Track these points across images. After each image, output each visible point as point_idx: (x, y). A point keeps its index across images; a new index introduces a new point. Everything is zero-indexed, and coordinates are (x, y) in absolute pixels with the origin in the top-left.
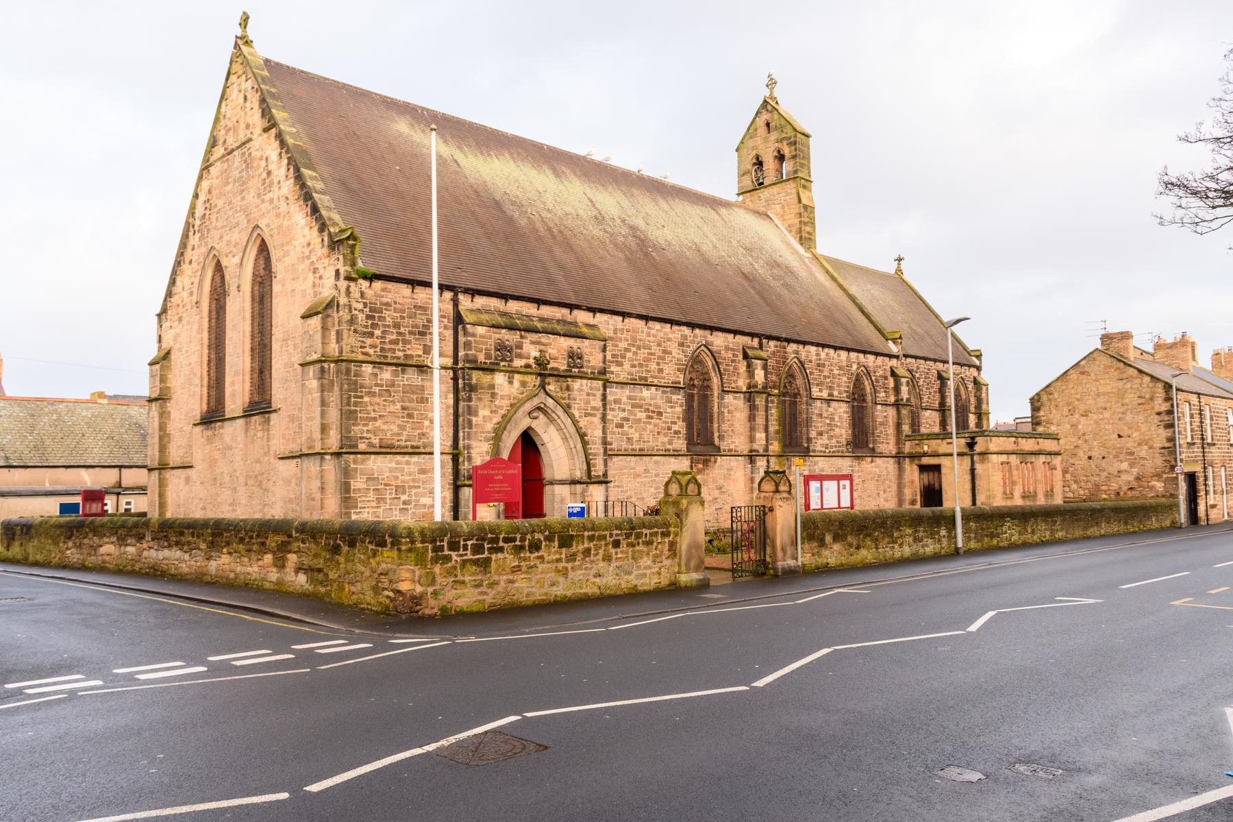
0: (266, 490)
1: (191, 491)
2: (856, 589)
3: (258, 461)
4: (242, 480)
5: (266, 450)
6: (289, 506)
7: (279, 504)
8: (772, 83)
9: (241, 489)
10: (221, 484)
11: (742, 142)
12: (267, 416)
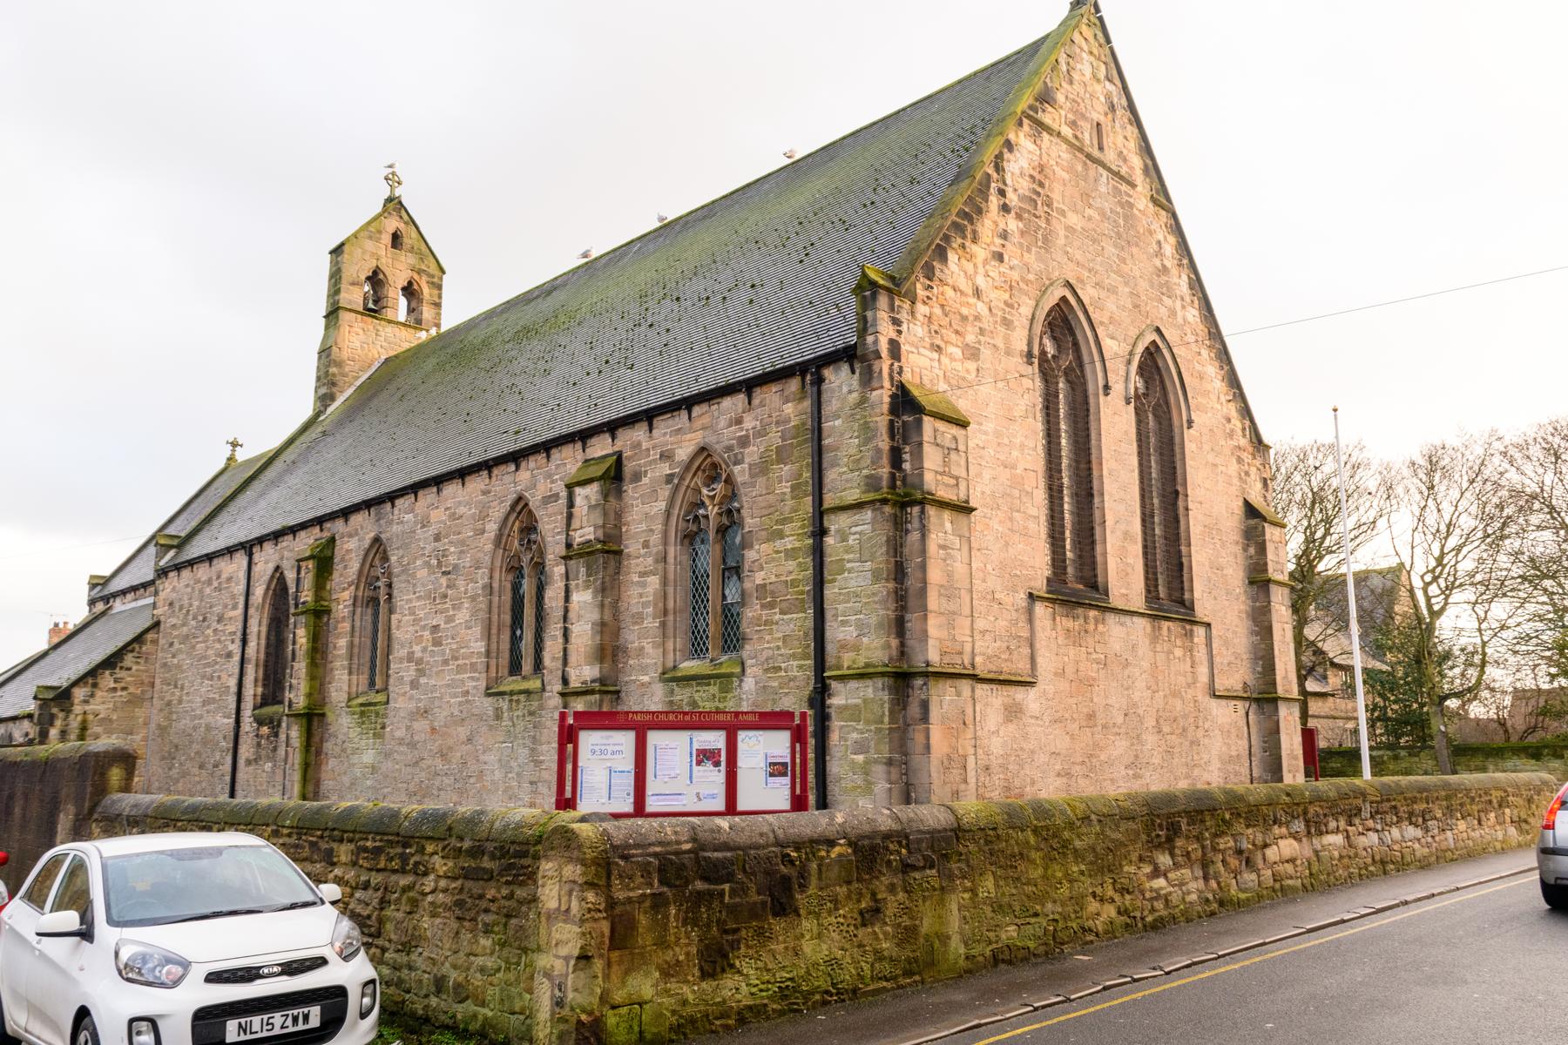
1: (1025, 737)
3: (1175, 694)
5: (1190, 680)
6: (1230, 768)
7: (1216, 764)
8: (392, 179)
9: (1150, 739)
10: (1104, 727)
11: (355, 235)
12: (1188, 627)
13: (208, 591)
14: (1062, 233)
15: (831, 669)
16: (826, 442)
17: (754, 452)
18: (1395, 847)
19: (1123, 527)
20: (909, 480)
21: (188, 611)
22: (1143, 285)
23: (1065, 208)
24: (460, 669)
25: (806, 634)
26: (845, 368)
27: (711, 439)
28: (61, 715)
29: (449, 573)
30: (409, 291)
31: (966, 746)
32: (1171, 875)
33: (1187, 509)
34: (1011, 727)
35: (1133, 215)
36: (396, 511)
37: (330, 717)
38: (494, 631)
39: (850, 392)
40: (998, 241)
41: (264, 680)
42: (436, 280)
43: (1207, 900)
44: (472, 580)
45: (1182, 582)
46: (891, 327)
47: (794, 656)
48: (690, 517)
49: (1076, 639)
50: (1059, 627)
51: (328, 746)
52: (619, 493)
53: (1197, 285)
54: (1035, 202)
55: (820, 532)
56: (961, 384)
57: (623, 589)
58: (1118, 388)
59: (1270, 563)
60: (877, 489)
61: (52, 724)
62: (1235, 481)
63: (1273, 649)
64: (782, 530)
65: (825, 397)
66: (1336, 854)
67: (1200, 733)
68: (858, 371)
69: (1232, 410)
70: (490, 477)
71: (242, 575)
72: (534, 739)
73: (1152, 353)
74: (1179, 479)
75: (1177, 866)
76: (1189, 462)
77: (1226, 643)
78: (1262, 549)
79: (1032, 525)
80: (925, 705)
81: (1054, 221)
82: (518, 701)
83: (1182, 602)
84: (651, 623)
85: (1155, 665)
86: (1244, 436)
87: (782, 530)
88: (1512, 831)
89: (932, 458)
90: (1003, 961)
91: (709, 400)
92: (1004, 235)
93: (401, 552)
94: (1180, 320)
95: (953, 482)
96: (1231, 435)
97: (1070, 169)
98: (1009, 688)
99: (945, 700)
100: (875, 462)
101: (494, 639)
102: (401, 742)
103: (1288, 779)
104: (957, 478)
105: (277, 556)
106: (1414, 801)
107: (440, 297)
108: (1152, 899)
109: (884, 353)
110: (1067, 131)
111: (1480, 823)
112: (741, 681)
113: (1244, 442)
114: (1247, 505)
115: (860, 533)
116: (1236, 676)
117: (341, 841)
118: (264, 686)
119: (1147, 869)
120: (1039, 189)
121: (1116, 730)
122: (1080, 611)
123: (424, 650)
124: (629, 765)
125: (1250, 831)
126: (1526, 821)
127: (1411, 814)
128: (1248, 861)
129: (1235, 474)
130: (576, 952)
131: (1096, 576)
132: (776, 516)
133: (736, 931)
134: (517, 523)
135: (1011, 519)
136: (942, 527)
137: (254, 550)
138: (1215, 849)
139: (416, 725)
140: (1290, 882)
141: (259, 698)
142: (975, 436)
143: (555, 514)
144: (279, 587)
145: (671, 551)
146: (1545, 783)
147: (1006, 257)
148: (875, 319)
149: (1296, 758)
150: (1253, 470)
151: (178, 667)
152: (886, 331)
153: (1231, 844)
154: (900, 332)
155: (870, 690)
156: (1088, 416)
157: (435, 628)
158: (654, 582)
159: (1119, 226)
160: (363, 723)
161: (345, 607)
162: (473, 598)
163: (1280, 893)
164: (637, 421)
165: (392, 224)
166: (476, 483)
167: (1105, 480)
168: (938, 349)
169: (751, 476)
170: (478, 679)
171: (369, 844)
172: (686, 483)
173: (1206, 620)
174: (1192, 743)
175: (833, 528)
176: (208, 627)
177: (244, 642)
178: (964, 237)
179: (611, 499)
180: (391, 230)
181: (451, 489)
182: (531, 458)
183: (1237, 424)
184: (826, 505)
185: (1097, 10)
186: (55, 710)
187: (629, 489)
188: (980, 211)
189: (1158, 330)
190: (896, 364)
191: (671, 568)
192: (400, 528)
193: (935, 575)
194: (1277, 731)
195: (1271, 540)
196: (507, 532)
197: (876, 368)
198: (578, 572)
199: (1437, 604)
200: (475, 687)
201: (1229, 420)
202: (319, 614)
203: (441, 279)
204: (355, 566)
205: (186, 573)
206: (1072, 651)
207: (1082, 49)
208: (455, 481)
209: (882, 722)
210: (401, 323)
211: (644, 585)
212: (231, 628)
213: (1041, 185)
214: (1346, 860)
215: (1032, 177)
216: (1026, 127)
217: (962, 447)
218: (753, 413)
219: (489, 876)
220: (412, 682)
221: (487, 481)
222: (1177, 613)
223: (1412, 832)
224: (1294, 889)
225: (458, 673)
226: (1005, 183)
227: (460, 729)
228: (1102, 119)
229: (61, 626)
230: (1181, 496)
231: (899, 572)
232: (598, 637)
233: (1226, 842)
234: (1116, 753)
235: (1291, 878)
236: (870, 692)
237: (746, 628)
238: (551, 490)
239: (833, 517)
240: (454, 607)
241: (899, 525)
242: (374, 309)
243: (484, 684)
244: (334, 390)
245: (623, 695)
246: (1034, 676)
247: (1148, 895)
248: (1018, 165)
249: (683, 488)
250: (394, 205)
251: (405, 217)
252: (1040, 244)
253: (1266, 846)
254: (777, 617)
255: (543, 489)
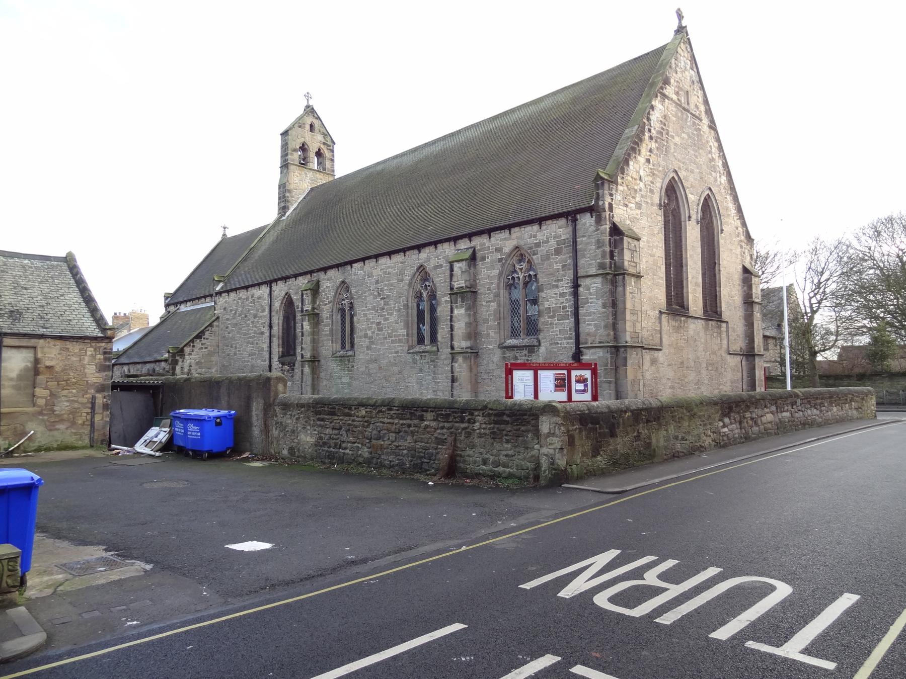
0: (721, 374)
1: (658, 372)
2: (884, 420)
4: (704, 365)
6: (734, 385)
8: (308, 96)
9: (704, 372)
12: (719, 323)
13: (246, 303)
14: (673, 147)
15: (583, 344)
16: (579, 247)
17: (543, 250)
18: (809, 418)
19: (694, 280)
20: (617, 264)
21: (236, 313)
22: (704, 167)
23: (674, 135)
24: (393, 342)
25: (570, 329)
26: (588, 215)
27: (522, 243)
28: (181, 360)
29: (385, 298)
30: (319, 154)
31: (640, 376)
32: (729, 427)
33: (720, 271)
34: (653, 368)
35: (700, 134)
36: (353, 270)
37: (322, 362)
38: (410, 325)
39: (591, 225)
40: (648, 154)
41: (282, 345)
42: (331, 148)
43: (741, 437)
44: (397, 303)
45: (716, 303)
46: (609, 197)
47: (565, 338)
48: (510, 277)
49: (678, 329)
50: (670, 325)
51: (322, 375)
52: (475, 265)
53: (726, 165)
54: (662, 133)
55: (576, 286)
56: (634, 220)
57: (478, 308)
58: (694, 217)
59: (753, 294)
60: (604, 268)
61: (177, 364)
62: (739, 256)
63: (753, 333)
64: (558, 285)
65: (578, 227)
66: (787, 420)
67: (723, 370)
68: (594, 217)
69: (738, 223)
70: (405, 256)
71: (266, 296)
72: (434, 373)
73: (707, 200)
74: (716, 257)
75: (731, 423)
76: (721, 249)
77: (734, 331)
78: (750, 287)
79: (660, 281)
80: (625, 359)
81: (670, 141)
82: (425, 356)
83: (716, 312)
84: (493, 323)
85: (706, 340)
86: (743, 235)
87: (558, 285)
88: (855, 412)
89: (627, 256)
90: (676, 457)
91: (520, 226)
92: (651, 151)
93: (357, 288)
94: (719, 183)
95: (635, 265)
96: (738, 235)
97: (676, 116)
98: (651, 351)
99: (633, 357)
100: (604, 256)
101: (410, 328)
102: (362, 373)
103: (758, 390)
104: (636, 263)
105: (286, 288)
106: (817, 398)
107: (333, 156)
108: (723, 436)
109: (607, 209)
110: (675, 97)
111: (842, 409)
112: (539, 348)
113: (743, 238)
114: (744, 267)
115: (596, 287)
116: (739, 344)
117: (427, 411)
118: (283, 347)
119: (721, 424)
120: (664, 127)
121: (691, 369)
122: (678, 318)
123: (373, 333)
124: (532, 384)
125: (756, 410)
126: (860, 408)
127: (816, 404)
128: (755, 422)
129: (739, 253)
130: (559, 447)
131: (683, 302)
132: (555, 278)
133: (601, 441)
134: (419, 277)
135: (653, 279)
136: (631, 283)
137: (273, 285)
138: (744, 418)
139: (371, 366)
140: (770, 431)
141: (281, 353)
142: (642, 243)
143: (441, 274)
144: (289, 303)
145: (502, 291)
146: (869, 391)
147: (651, 160)
148: (603, 194)
149: (761, 380)
150: (747, 251)
151: (233, 338)
152: (608, 200)
153: (750, 415)
154: (612, 199)
155: (601, 353)
156: (681, 230)
157: (379, 323)
158: (494, 305)
159: (695, 140)
160: (342, 365)
161: (327, 312)
162: (398, 310)
163: (766, 434)
164: (483, 234)
165: (309, 120)
166: (398, 258)
167: (688, 260)
168: (626, 206)
169: (542, 260)
170: (403, 346)
171: (443, 412)
172: (508, 262)
173: (726, 320)
174: (720, 374)
175: (583, 284)
176: (249, 320)
177: (271, 327)
178: (635, 153)
179: (472, 268)
180: (309, 123)
181: (383, 261)
182: (427, 248)
183: (740, 230)
184: (579, 275)
185: (687, 35)
186: (178, 358)
187: (479, 264)
188: (641, 140)
189: (710, 189)
190: (611, 214)
191: (502, 300)
192: (356, 277)
193: (629, 305)
194: (754, 369)
195: (755, 284)
196: (414, 281)
197: (603, 216)
198: (457, 301)
199: (815, 306)
200: (401, 350)
201: (737, 228)
202: (315, 317)
203: (333, 147)
204: (331, 294)
205: (233, 295)
206: (675, 335)
207: (681, 56)
208: (385, 257)
209: (607, 366)
210: (315, 170)
211: (489, 306)
212: (261, 321)
213: (665, 125)
214: (790, 423)
215: (661, 121)
216: (659, 98)
217: (638, 250)
218: (542, 233)
219: (507, 423)
220: (367, 347)
221: (403, 258)
222: (715, 317)
223: (815, 411)
224: (771, 433)
225: (392, 343)
226: (651, 126)
227: (395, 368)
228: (689, 89)
229: (118, 314)
230: (717, 265)
231: (614, 304)
232: (469, 329)
233: (748, 415)
234: (691, 378)
235: (770, 429)
236: (601, 354)
237: (540, 326)
238: (438, 263)
239: (582, 279)
240: (388, 314)
241: (614, 283)
242: (304, 163)
243: (407, 348)
244: (288, 204)
245: (480, 353)
246: (661, 346)
247: (722, 434)
248: (655, 116)
249: (507, 265)
250: (310, 110)
251: (316, 115)
252: (664, 153)
253: (762, 416)
254: (556, 321)
255: (433, 262)
